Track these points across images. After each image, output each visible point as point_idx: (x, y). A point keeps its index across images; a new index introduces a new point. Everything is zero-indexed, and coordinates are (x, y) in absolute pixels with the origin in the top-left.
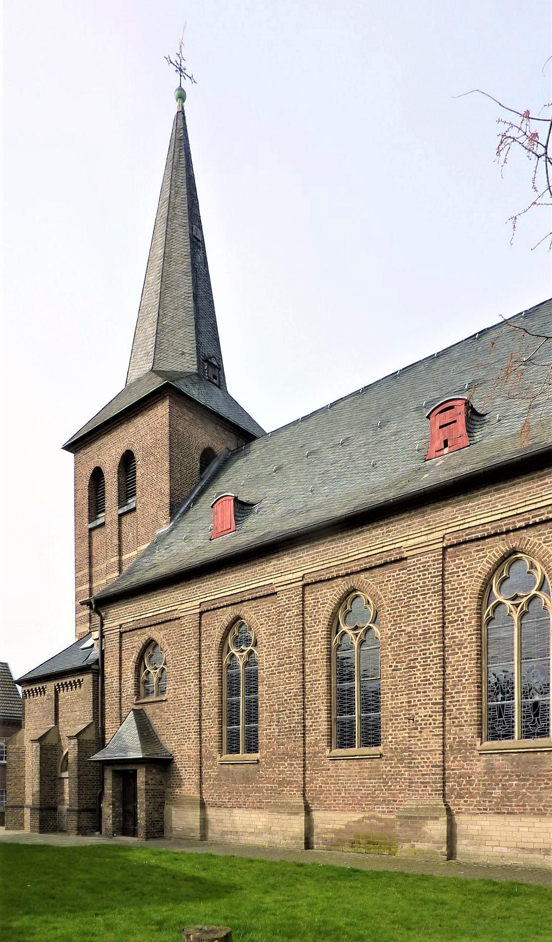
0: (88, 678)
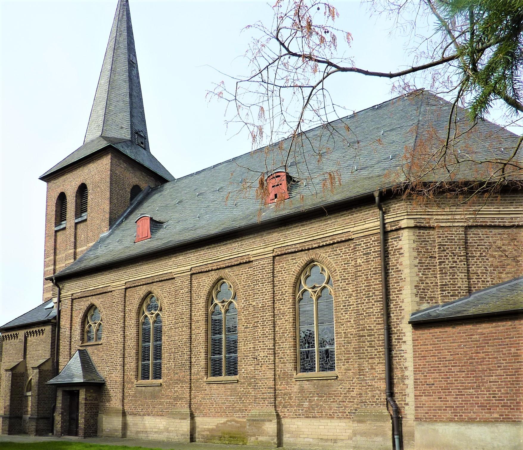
0: (48, 329)
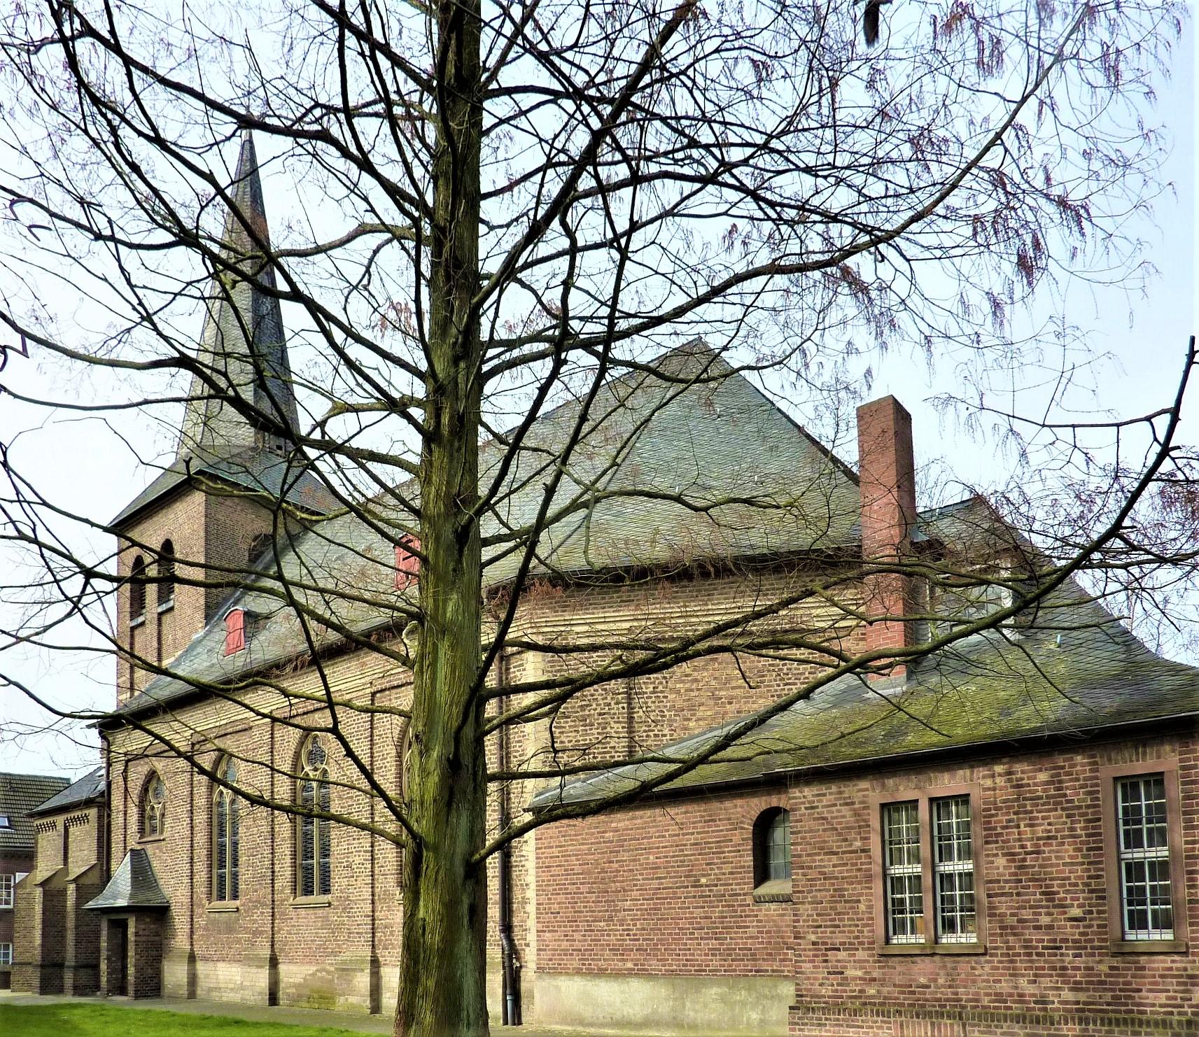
0: (93, 813)
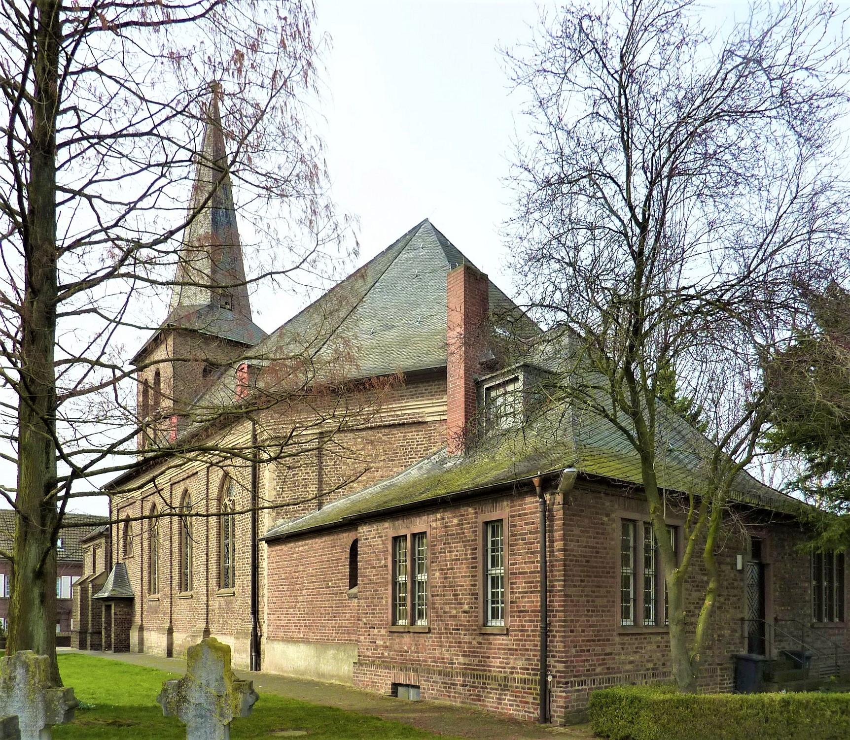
0: (103, 540)
